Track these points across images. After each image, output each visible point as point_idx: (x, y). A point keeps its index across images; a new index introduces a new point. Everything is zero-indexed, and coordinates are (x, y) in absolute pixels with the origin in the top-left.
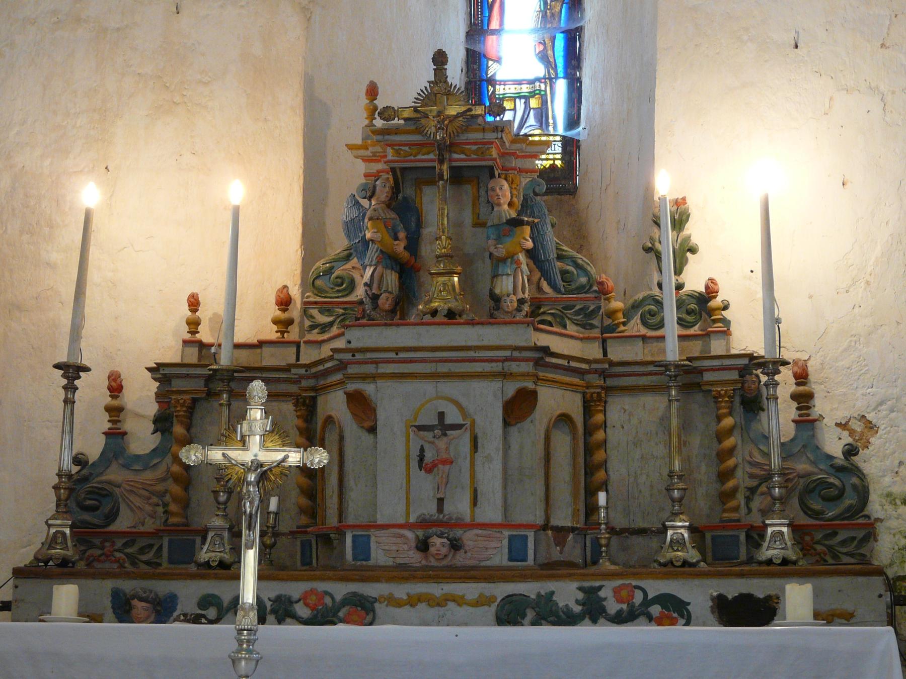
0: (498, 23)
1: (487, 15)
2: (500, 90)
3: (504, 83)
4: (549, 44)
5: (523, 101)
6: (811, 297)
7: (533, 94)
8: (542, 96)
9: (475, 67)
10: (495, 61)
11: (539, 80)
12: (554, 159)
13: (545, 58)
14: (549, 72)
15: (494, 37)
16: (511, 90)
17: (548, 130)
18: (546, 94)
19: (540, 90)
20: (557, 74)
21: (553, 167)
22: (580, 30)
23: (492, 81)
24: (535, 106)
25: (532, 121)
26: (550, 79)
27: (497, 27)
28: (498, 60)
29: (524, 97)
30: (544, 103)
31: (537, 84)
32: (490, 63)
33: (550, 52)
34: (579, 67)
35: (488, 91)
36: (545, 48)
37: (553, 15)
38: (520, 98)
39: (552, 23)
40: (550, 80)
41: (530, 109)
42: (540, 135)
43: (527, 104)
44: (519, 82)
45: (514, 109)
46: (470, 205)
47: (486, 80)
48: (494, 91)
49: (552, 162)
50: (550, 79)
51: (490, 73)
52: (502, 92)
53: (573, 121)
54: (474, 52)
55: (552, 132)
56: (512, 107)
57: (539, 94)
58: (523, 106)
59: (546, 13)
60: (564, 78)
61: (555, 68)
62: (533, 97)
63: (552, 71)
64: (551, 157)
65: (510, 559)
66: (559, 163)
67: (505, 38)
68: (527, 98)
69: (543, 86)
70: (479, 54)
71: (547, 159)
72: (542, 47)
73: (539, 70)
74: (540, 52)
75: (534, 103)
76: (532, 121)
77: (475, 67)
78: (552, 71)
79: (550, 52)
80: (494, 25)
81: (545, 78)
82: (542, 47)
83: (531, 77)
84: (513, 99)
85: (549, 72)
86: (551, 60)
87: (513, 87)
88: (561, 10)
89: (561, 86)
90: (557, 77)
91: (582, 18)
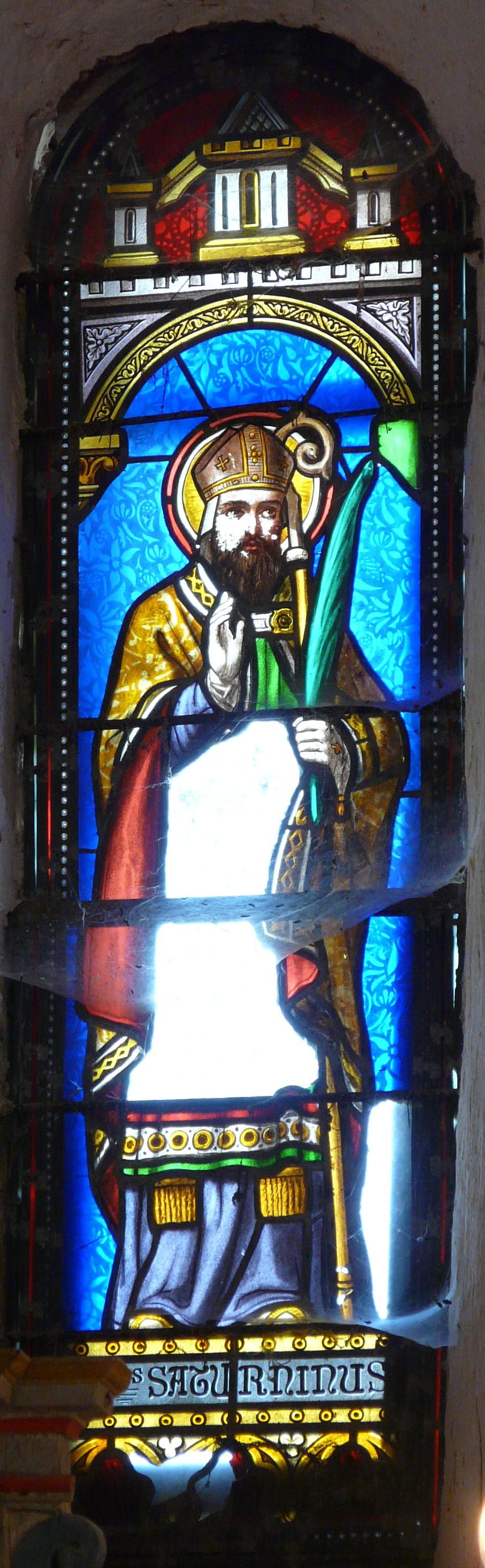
0: (136, 876)
1: (94, 843)
2: (140, 1144)
3: (157, 1113)
4: (338, 957)
5: (231, 1190)
6: (5, 612)
7: (269, 1163)
8: (308, 1168)
9: (41, 1053)
10: (120, 1029)
11: (292, 1100)
12: (354, 1427)
13: (318, 1010)
14: (338, 1073)
15: (121, 933)
16: (184, 1142)
17: (330, 1304)
18: (324, 1164)
19: (302, 1146)
20: (369, 1078)
21: (349, 1454)
22: (453, 897)
23: (114, 1111)
24: (281, 1211)
25: (265, 1271)
26: (343, 1099)
27: (134, 894)
28: (138, 1027)
29: (235, 1174)
30: (315, 1195)
31: (290, 1120)
32: (105, 1036)
33: (343, 992)
34: (451, 1051)
35: (93, 1149)
36: (324, 975)
37: (356, 843)
38: (221, 1176)
39: (352, 873)
40: (340, 1101)
41: (262, 1221)
42: (297, 1329)
43: (247, 1201)
44: (216, 1112)
45: (196, 1226)
46: (383, 172)
47: (82, 1108)
48: (116, 1150)
49: (342, 1439)
50: (343, 1099)
51: (105, 1074)
52: (146, 1153)
53: (423, 1272)
54: (38, 993)
55: (346, 1316)
56: (186, 1213)
57: (295, 1161)
58: (230, 1208)
59: (330, 831)
60: (394, 1095)
61: (364, 1055)
62: (272, 1173)
63: (349, 1069)
64: (342, 1416)
65: (242, 148)
66: (370, 1441)
67: (168, 938)
68: (246, 1180)
69: (312, 1129)
70: (60, 1000)
71: (324, 1427)
72: (309, 973)
73: (295, 1063)
74: (302, 991)
75: (274, 1198)
76: (265, 1271)
77: (41, 1053)
78: (349, 1069)
79: (343, 992)
80: (124, 884)
81: (319, 1093)
82: (309, 973)
83: (267, 1089)
84: (192, 1183)
85: (338, 1073)
86: (348, 1022)
87: (190, 1133)
88: (390, 819)
89: (385, 1127)
90: (370, 1095)
91: (458, 852)
